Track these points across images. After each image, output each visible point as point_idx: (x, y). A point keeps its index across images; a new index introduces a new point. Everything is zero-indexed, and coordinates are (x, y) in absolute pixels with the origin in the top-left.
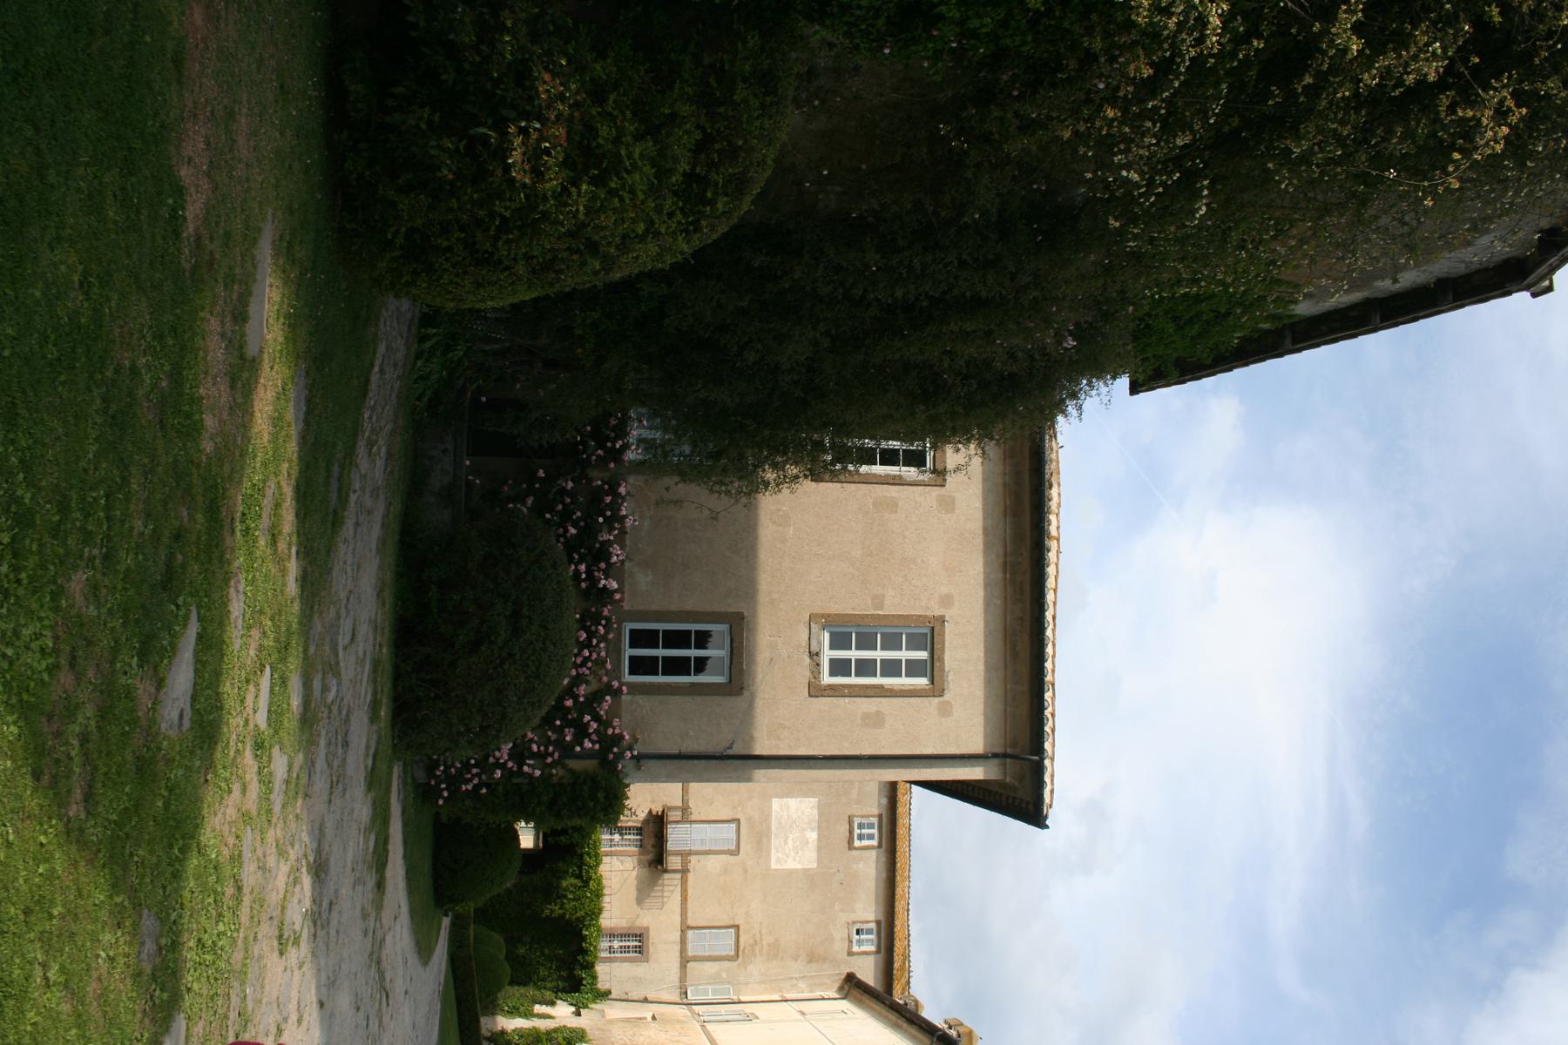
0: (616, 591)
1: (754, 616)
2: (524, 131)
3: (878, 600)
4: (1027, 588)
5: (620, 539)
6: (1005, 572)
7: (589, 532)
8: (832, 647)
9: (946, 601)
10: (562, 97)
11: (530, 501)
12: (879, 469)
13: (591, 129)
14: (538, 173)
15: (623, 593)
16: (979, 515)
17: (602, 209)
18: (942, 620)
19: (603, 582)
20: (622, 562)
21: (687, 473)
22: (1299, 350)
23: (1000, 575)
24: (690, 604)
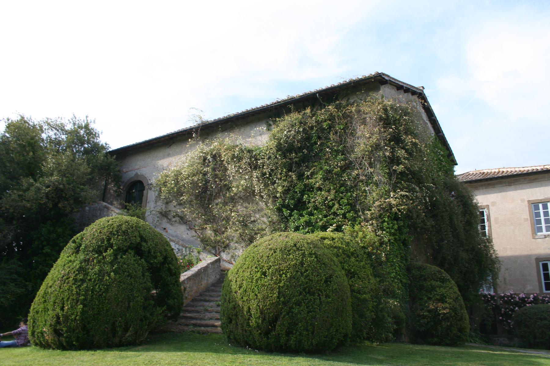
0: (534, 295)
1: (536, 255)
2: (440, 310)
3: (526, 220)
4: (515, 179)
5: (518, 295)
6: (511, 185)
7: (516, 304)
8: (542, 231)
9: (523, 201)
10: (432, 304)
11: (509, 321)
12: (487, 230)
13: (437, 299)
14: (446, 308)
15: (534, 293)
16: (496, 194)
17: (450, 297)
18: (529, 201)
19: (531, 299)
20: (524, 294)
21: (495, 276)
22: (442, 131)
23: (513, 186)
24: (535, 273)
